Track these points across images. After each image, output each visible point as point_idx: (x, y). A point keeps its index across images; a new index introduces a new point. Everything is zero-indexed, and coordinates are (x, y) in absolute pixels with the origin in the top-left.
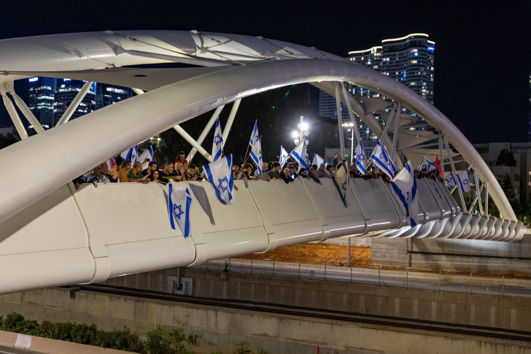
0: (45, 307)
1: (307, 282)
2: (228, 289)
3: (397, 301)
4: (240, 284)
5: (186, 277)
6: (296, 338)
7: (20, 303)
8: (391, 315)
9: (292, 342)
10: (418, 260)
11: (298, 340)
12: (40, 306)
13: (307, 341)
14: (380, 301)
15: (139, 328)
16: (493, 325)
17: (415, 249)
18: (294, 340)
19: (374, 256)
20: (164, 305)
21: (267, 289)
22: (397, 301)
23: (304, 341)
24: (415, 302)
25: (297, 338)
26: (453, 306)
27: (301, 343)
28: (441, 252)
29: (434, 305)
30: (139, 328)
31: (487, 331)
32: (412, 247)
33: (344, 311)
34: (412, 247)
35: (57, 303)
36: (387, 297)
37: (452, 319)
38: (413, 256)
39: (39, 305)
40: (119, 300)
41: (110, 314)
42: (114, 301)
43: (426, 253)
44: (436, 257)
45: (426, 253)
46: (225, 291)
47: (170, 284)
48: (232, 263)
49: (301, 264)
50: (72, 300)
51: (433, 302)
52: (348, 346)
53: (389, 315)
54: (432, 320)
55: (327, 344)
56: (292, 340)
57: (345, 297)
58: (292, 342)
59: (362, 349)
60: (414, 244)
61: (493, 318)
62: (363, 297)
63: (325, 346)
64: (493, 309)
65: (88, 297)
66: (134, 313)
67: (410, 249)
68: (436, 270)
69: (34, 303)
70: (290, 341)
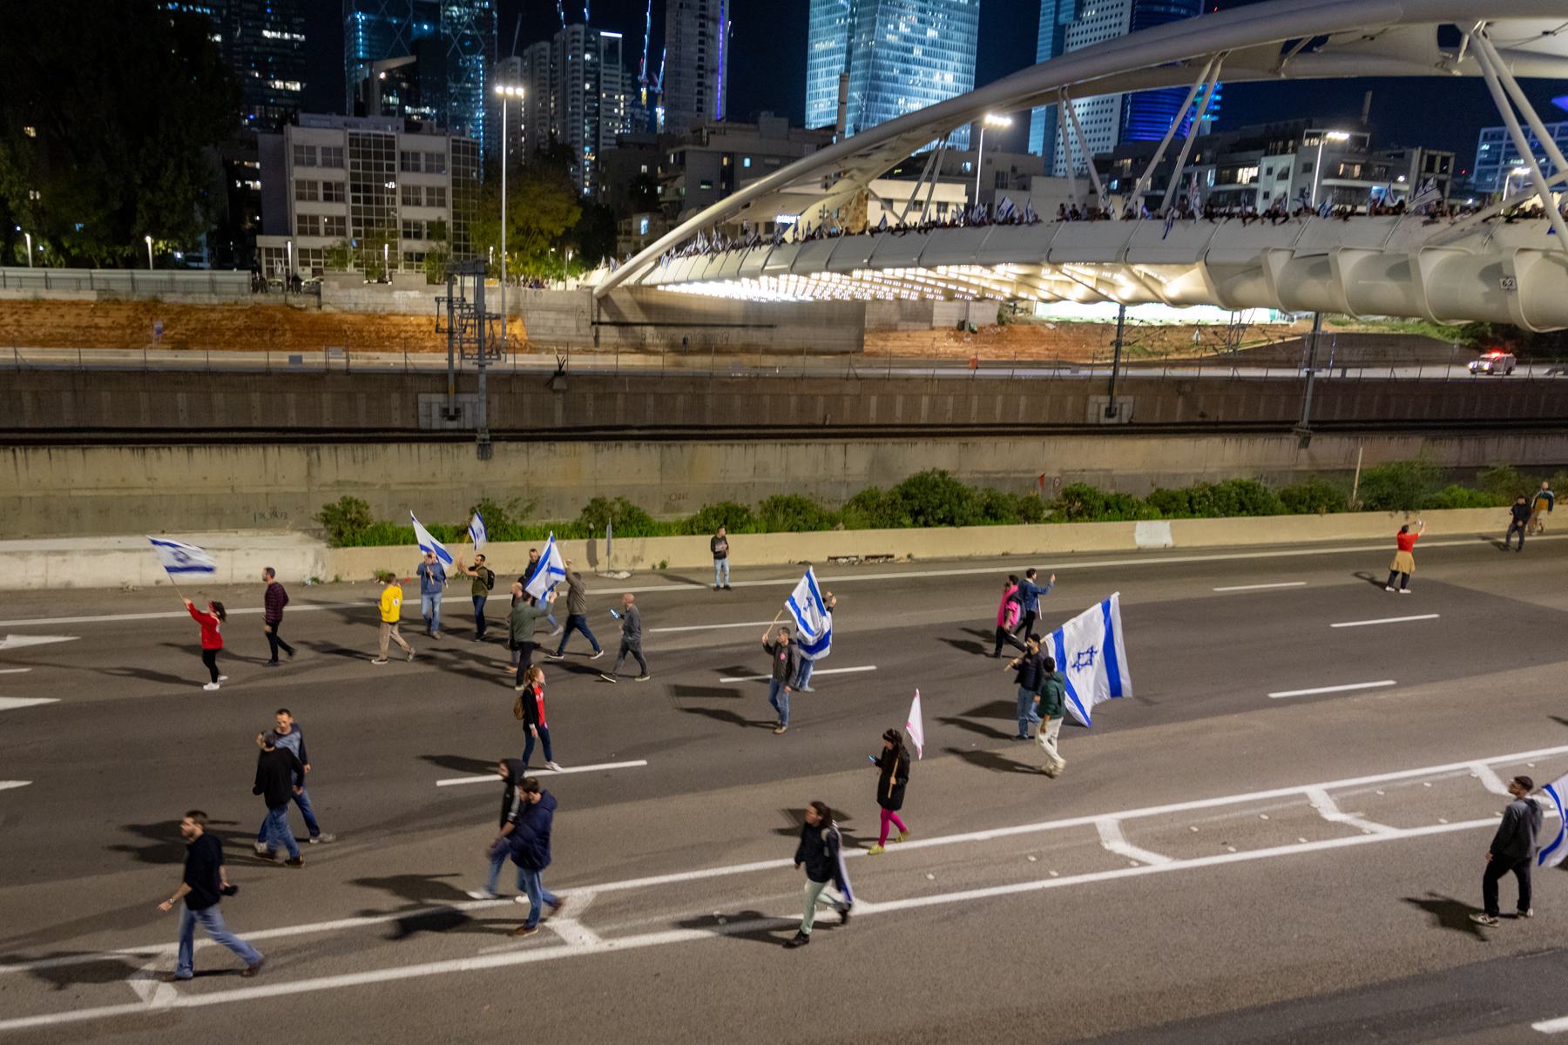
0: (393, 487)
1: (728, 384)
2: (565, 409)
3: (874, 400)
4: (592, 396)
5: (466, 392)
6: (987, 469)
7: (304, 489)
8: (865, 422)
9: (981, 476)
10: (610, 335)
11: (989, 473)
12: (377, 487)
13: (1002, 472)
14: (847, 403)
15: (673, 497)
16: (998, 420)
17: (605, 318)
18: (985, 472)
19: (533, 334)
20: (732, 445)
21: (651, 400)
22: (874, 400)
23: (999, 472)
24: (900, 399)
25: (988, 468)
26: (950, 399)
27: (995, 476)
28: (645, 321)
29: (925, 400)
30: (673, 497)
31: (859, 430)
32: (599, 316)
33: (790, 423)
34: (599, 316)
35: (434, 475)
36: (858, 396)
37: (948, 418)
38: (602, 329)
39: (374, 485)
40: (618, 448)
41: (596, 480)
42: (605, 451)
43: (622, 324)
44: (638, 329)
45: (622, 324)
46: (1241, 410)
47: (1092, 409)
48: (86, 357)
49: (408, 355)
50: (482, 464)
51: (924, 397)
52: (1065, 468)
53: (861, 422)
54: (922, 422)
55: (1034, 471)
56: (979, 472)
57: (793, 401)
58: (981, 476)
59: (1084, 470)
60: (602, 310)
61: (950, 415)
62: (821, 400)
63: (1032, 475)
64: (1000, 398)
65: (531, 451)
66: (661, 469)
67: (595, 319)
68: (641, 348)
69: (356, 483)
70: (976, 475)
